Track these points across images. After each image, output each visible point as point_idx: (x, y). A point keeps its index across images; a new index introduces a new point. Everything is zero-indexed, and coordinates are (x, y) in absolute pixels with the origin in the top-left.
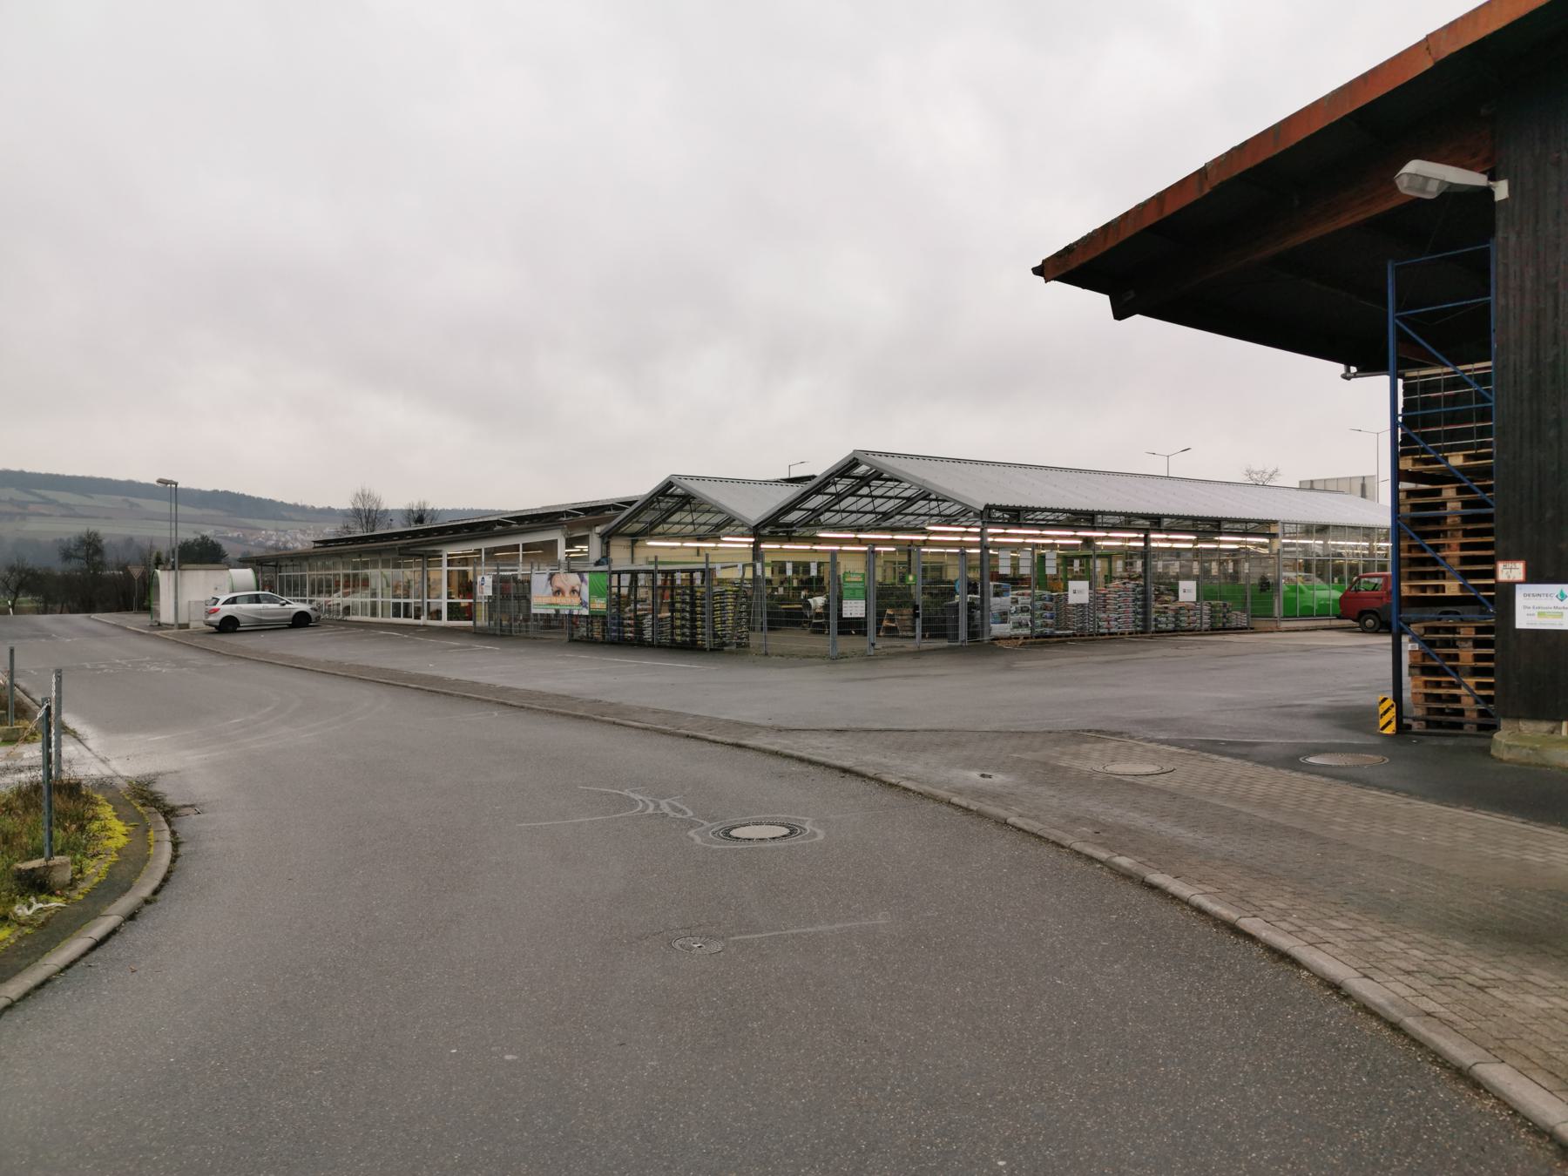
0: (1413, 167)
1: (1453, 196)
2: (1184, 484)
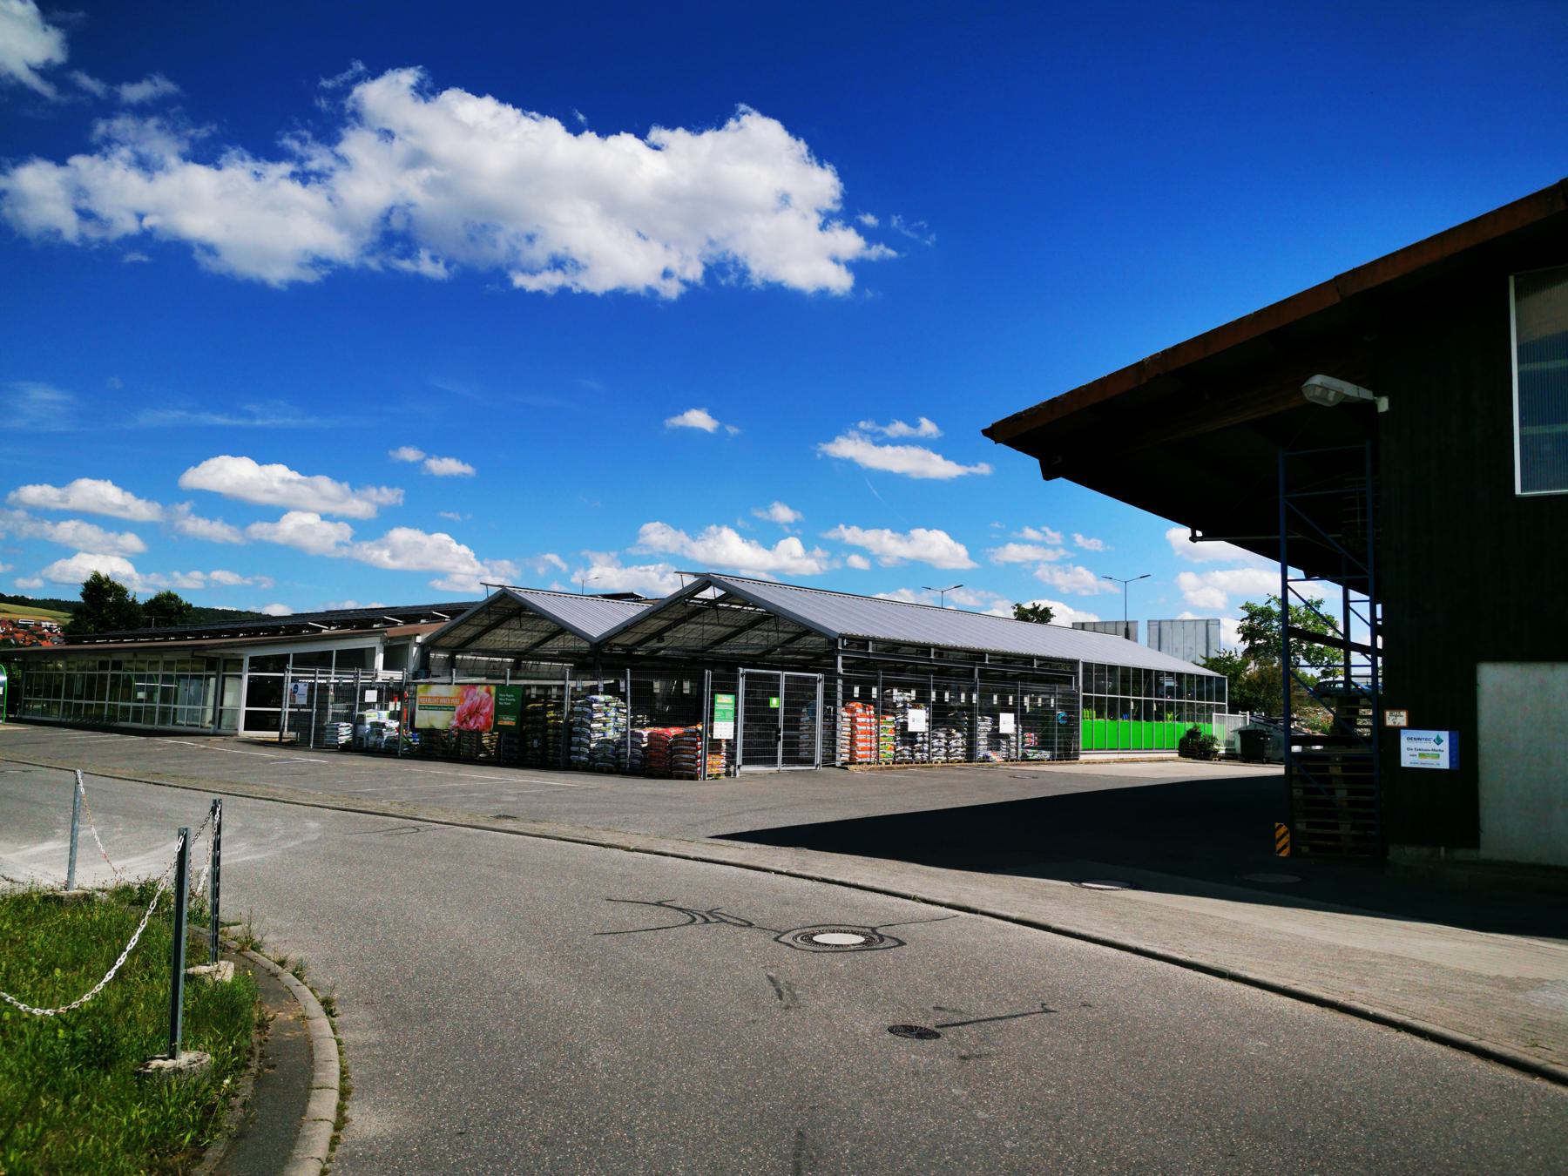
0: (1317, 380)
2: (970, 617)
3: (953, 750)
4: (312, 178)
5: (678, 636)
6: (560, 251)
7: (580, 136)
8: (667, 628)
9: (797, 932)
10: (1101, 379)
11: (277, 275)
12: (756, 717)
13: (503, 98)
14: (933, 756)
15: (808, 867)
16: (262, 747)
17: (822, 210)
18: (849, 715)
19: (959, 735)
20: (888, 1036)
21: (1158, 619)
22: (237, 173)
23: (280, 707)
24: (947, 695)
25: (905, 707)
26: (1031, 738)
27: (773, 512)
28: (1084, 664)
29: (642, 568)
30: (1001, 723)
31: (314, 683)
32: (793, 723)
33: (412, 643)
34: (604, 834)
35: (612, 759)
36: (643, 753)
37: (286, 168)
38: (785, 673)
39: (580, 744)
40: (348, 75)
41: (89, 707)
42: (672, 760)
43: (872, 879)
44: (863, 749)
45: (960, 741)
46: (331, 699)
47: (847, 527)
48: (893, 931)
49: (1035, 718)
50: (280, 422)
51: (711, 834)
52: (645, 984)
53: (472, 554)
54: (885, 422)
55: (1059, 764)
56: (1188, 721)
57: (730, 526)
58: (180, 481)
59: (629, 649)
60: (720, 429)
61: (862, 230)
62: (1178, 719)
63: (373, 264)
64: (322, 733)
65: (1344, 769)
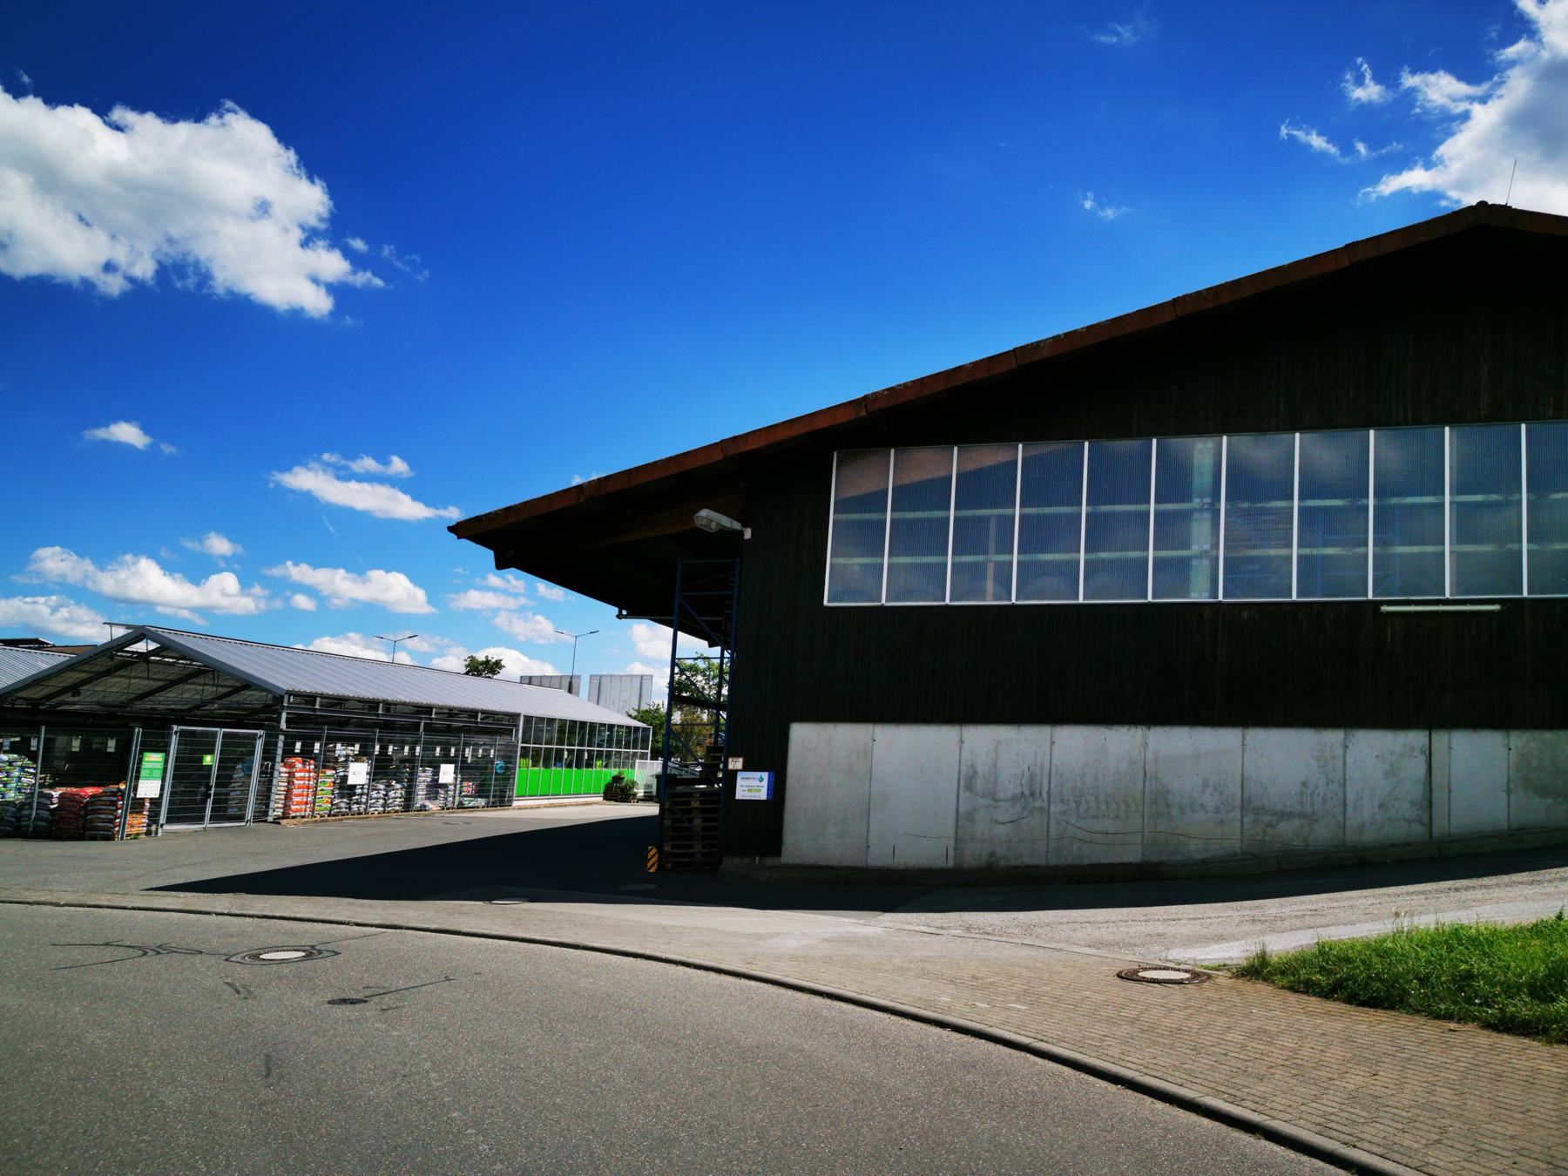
0: (704, 513)
1: (724, 533)
3: (391, 801)
5: (98, 689)
7: (21, 100)
9: (245, 954)
10: (549, 495)
12: (187, 778)
14: (371, 807)
15: (249, 907)
17: (306, 227)
18: (287, 770)
19: (398, 786)
20: (327, 1006)
21: (600, 674)
24: (391, 748)
25: (346, 761)
26: (469, 787)
27: (207, 543)
28: (525, 716)
29: (29, 600)
30: (441, 774)
32: (225, 779)
34: (26, 893)
36: (51, 815)
38: (223, 730)
42: (85, 821)
43: (311, 912)
44: (298, 803)
45: (399, 792)
47: (296, 564)
48: (330, 947)
49: (476, 768)
51: (145, 887)
52: (116, 996)
54: (354, 456)
55: (493, 811)
56: (615, 767)
57: (149, 557)
59: (35, 703)
60: (153, 449)
61: (348, 253)
62: (606, 766)
65: (702, 803)
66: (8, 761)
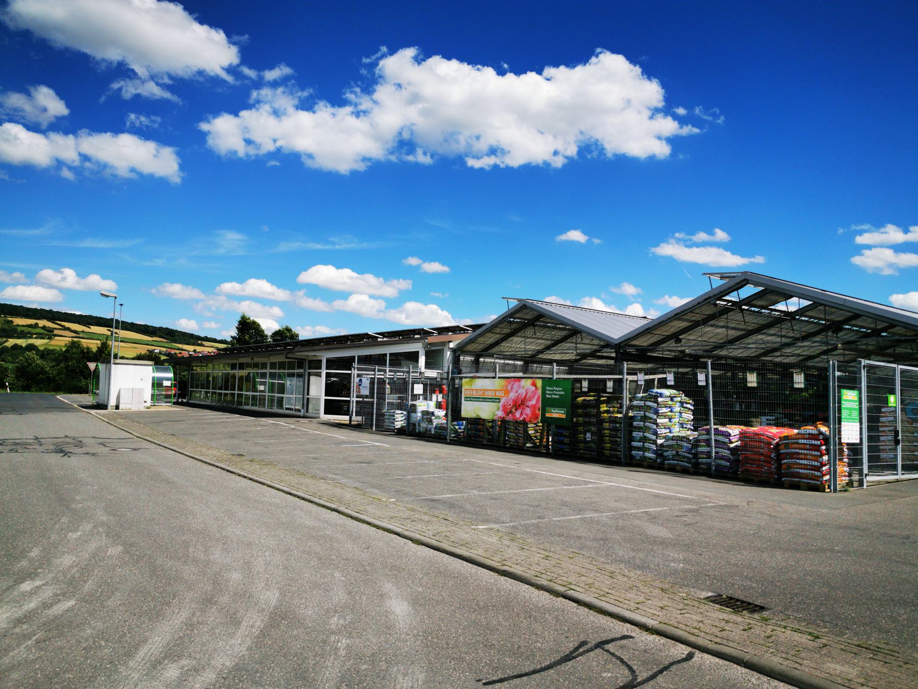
4: (361, 114)
5: (691, 338)
6: (494, 143)
8: (685, 331)
11: (344, 168)
13: (461, 60)
16: (336, 428)
22: (324, 112)
23: (349, 397)
31: (374, 378)
33: (446, 349)
35: (688, 458)
37: (348, 109)
39: (644, 439)
40: (379, 54)
41: (226, 395)
46: (388, 391)
47: (670, 297)
50: (348, 246)
53: (450, 316)
58: (297, 280)
60: (589, 241)
61: (676, 117)
63: (393, 158)
64: (382, 418)
66: (670, 396)
